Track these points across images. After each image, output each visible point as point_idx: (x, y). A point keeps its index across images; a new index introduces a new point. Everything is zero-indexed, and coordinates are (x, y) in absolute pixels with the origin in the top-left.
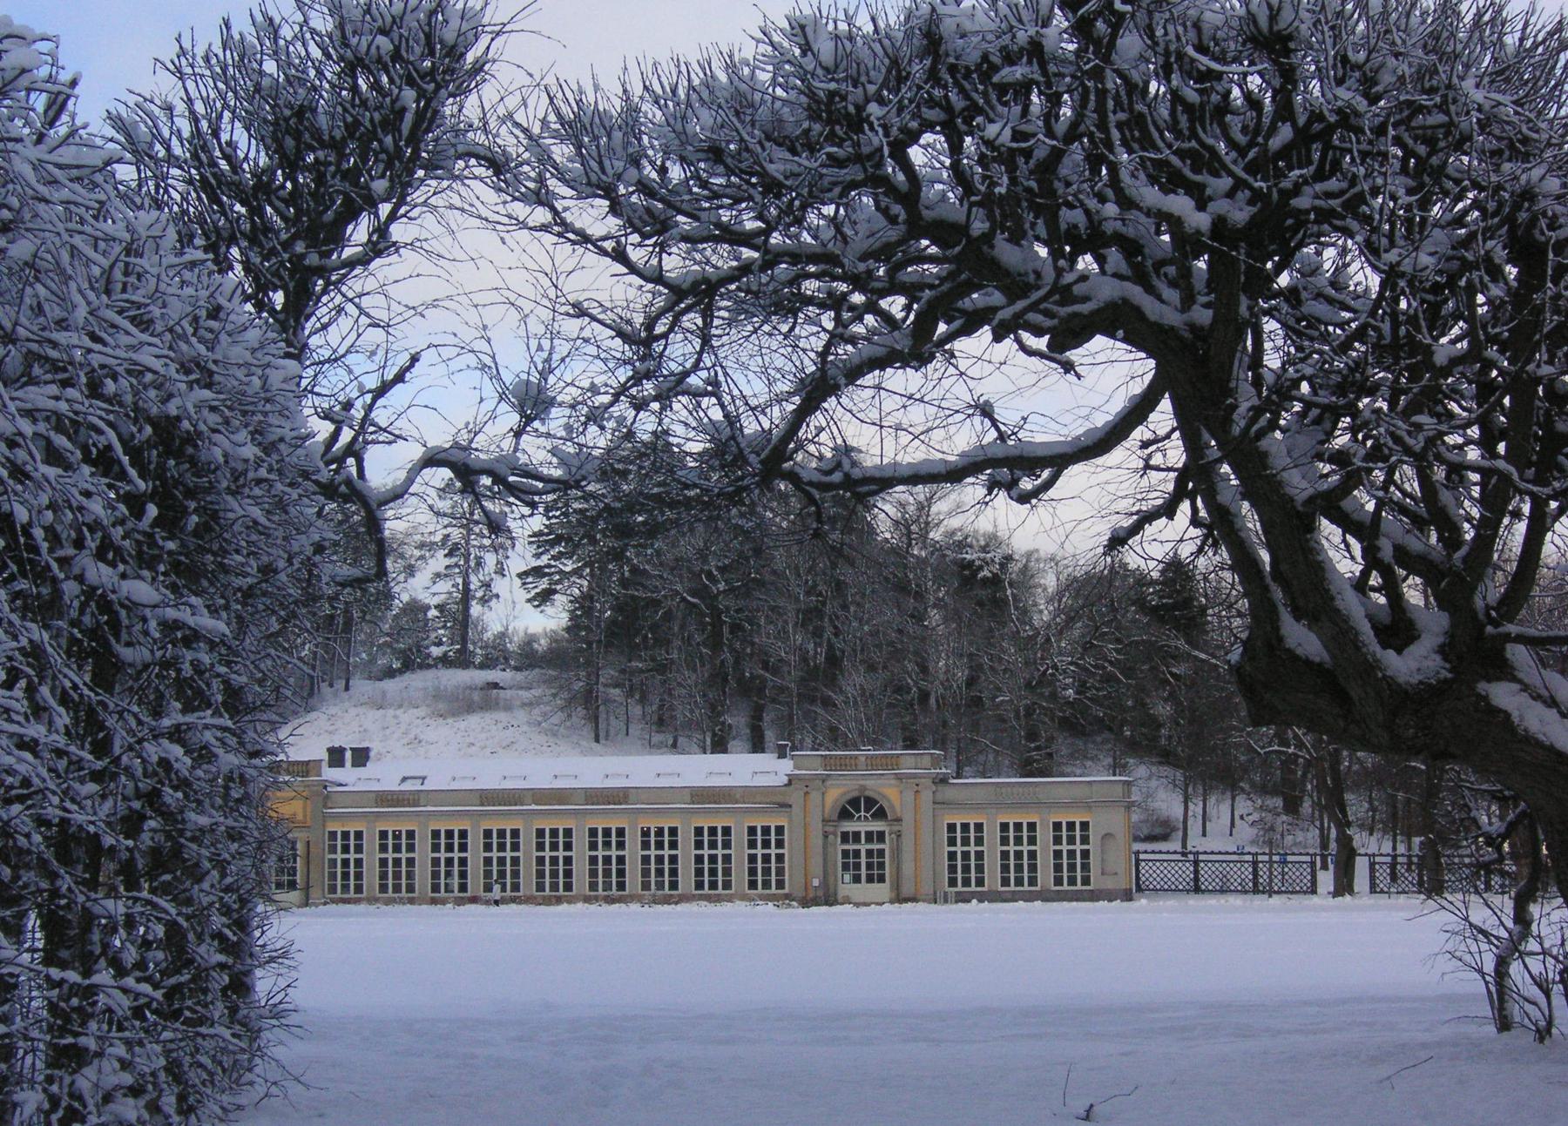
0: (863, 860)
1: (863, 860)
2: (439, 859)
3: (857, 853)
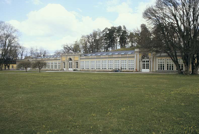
0: (146, 65)
1: (146, 65)
2: (131, 63)
3: (145, 64)
